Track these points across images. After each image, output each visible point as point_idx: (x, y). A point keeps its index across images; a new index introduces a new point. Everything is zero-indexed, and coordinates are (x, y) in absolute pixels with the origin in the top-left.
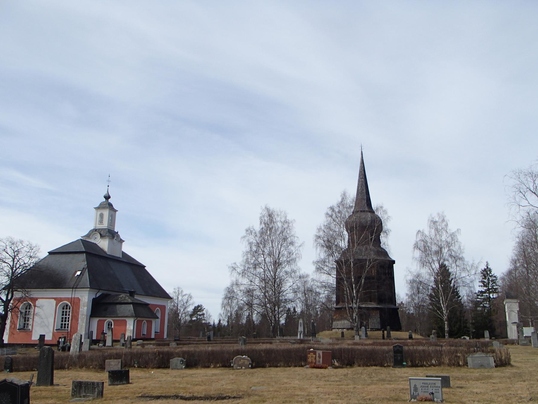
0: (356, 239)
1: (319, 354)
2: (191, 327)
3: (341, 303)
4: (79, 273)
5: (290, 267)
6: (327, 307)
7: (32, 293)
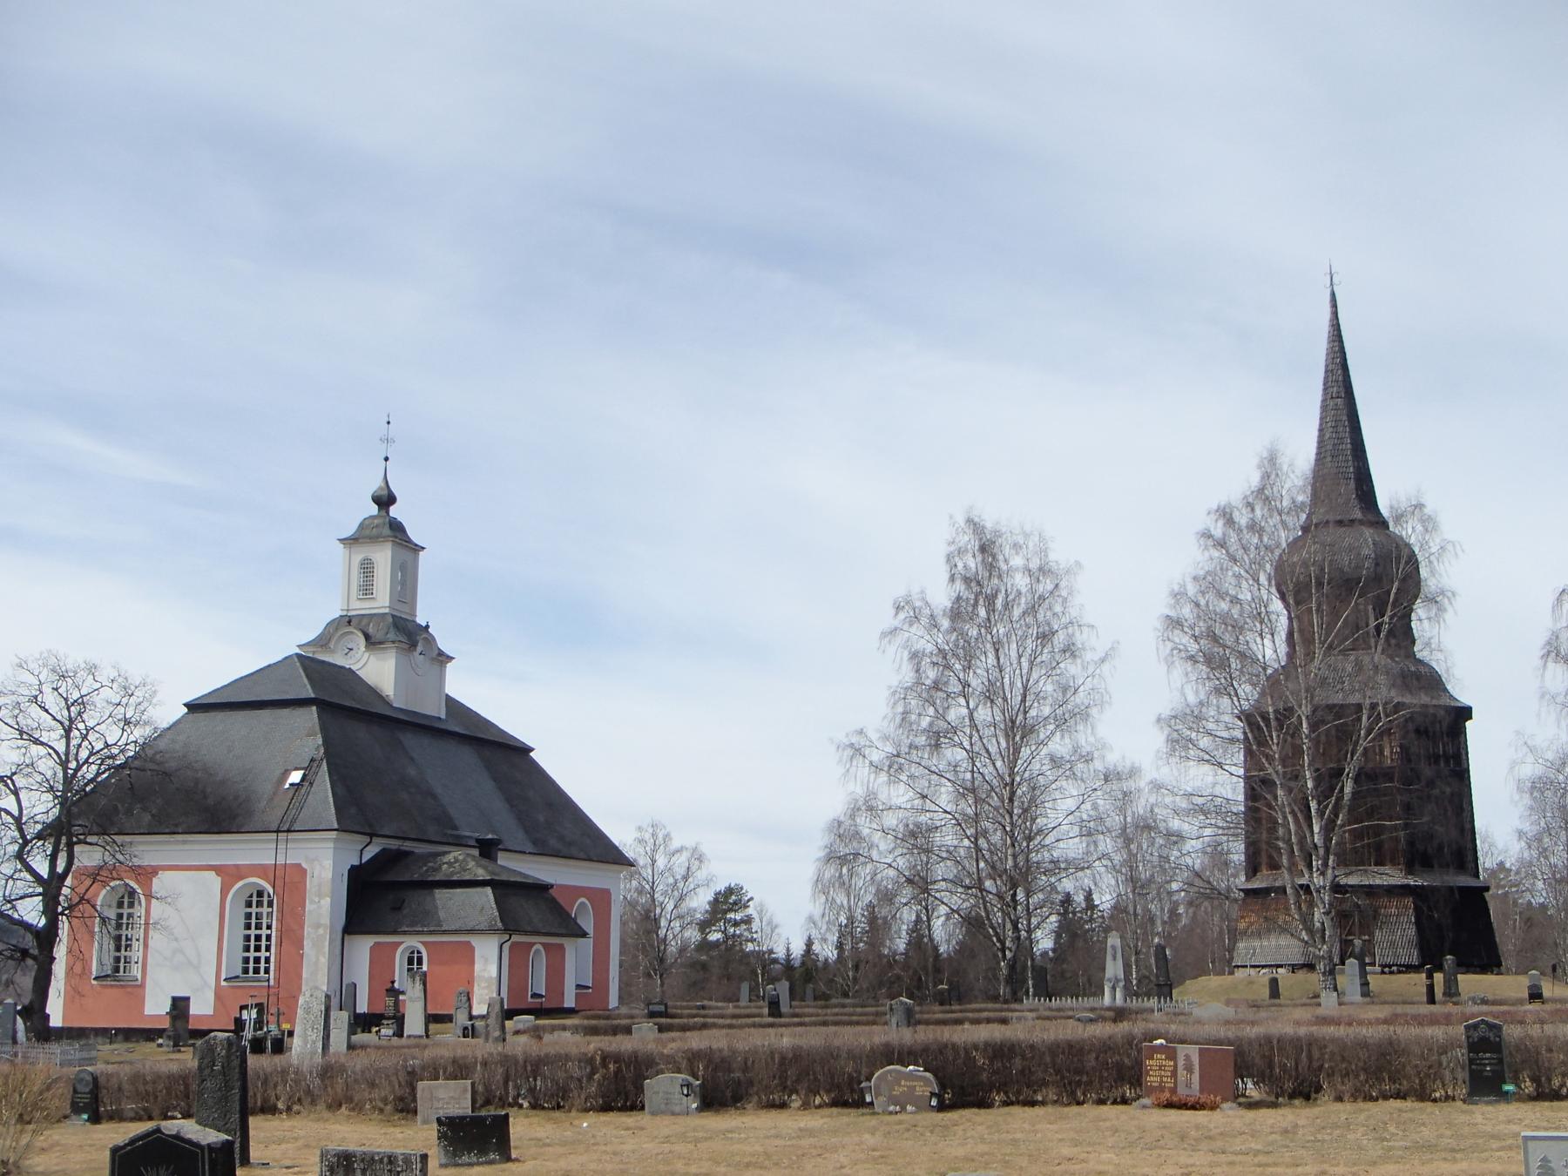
1: (1187, 1057)
2: (704, 967)
3: (1265, 872)
4: (296, 777)
5: (1067, 740)
6: (1213, 889)
7: (137, 849)
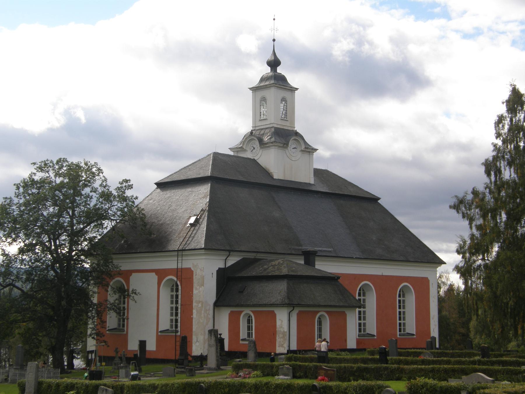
4: (192, 220)
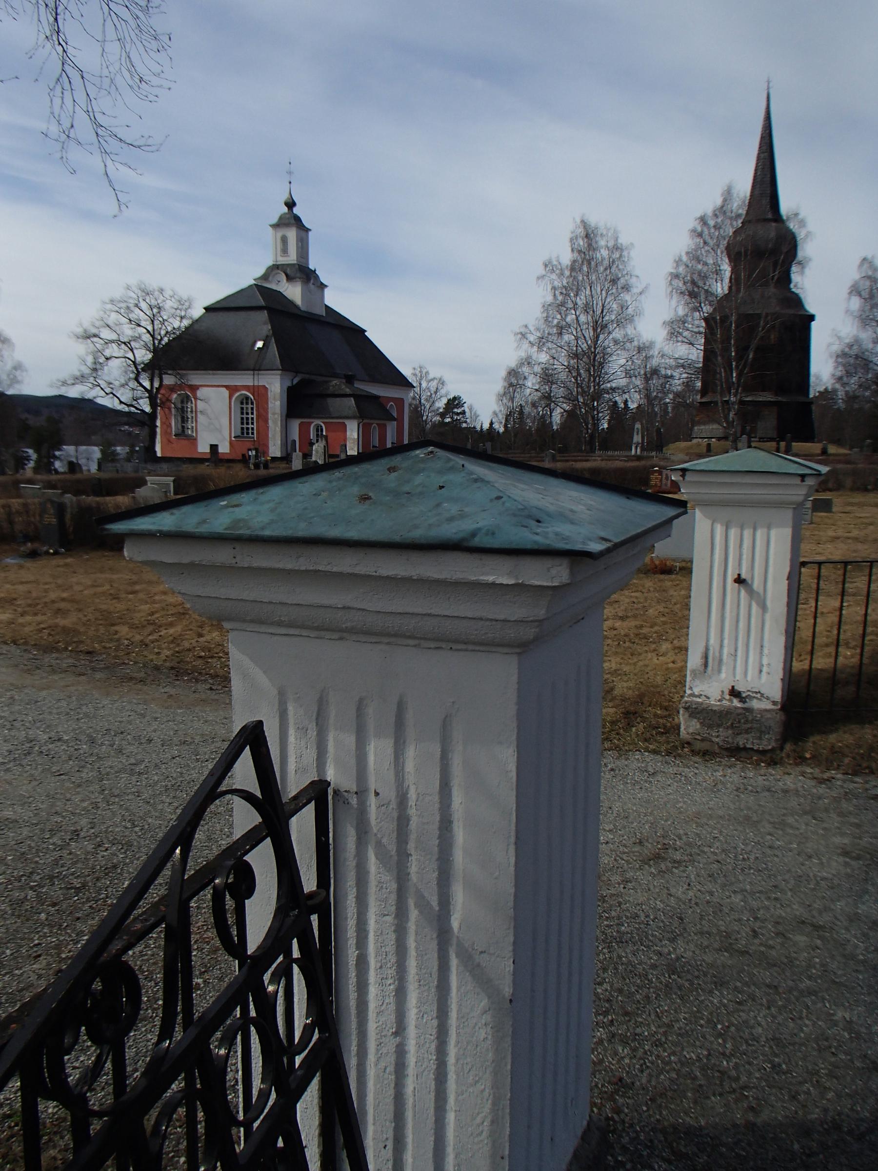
0: (744, 276)
4: (260, 344)
